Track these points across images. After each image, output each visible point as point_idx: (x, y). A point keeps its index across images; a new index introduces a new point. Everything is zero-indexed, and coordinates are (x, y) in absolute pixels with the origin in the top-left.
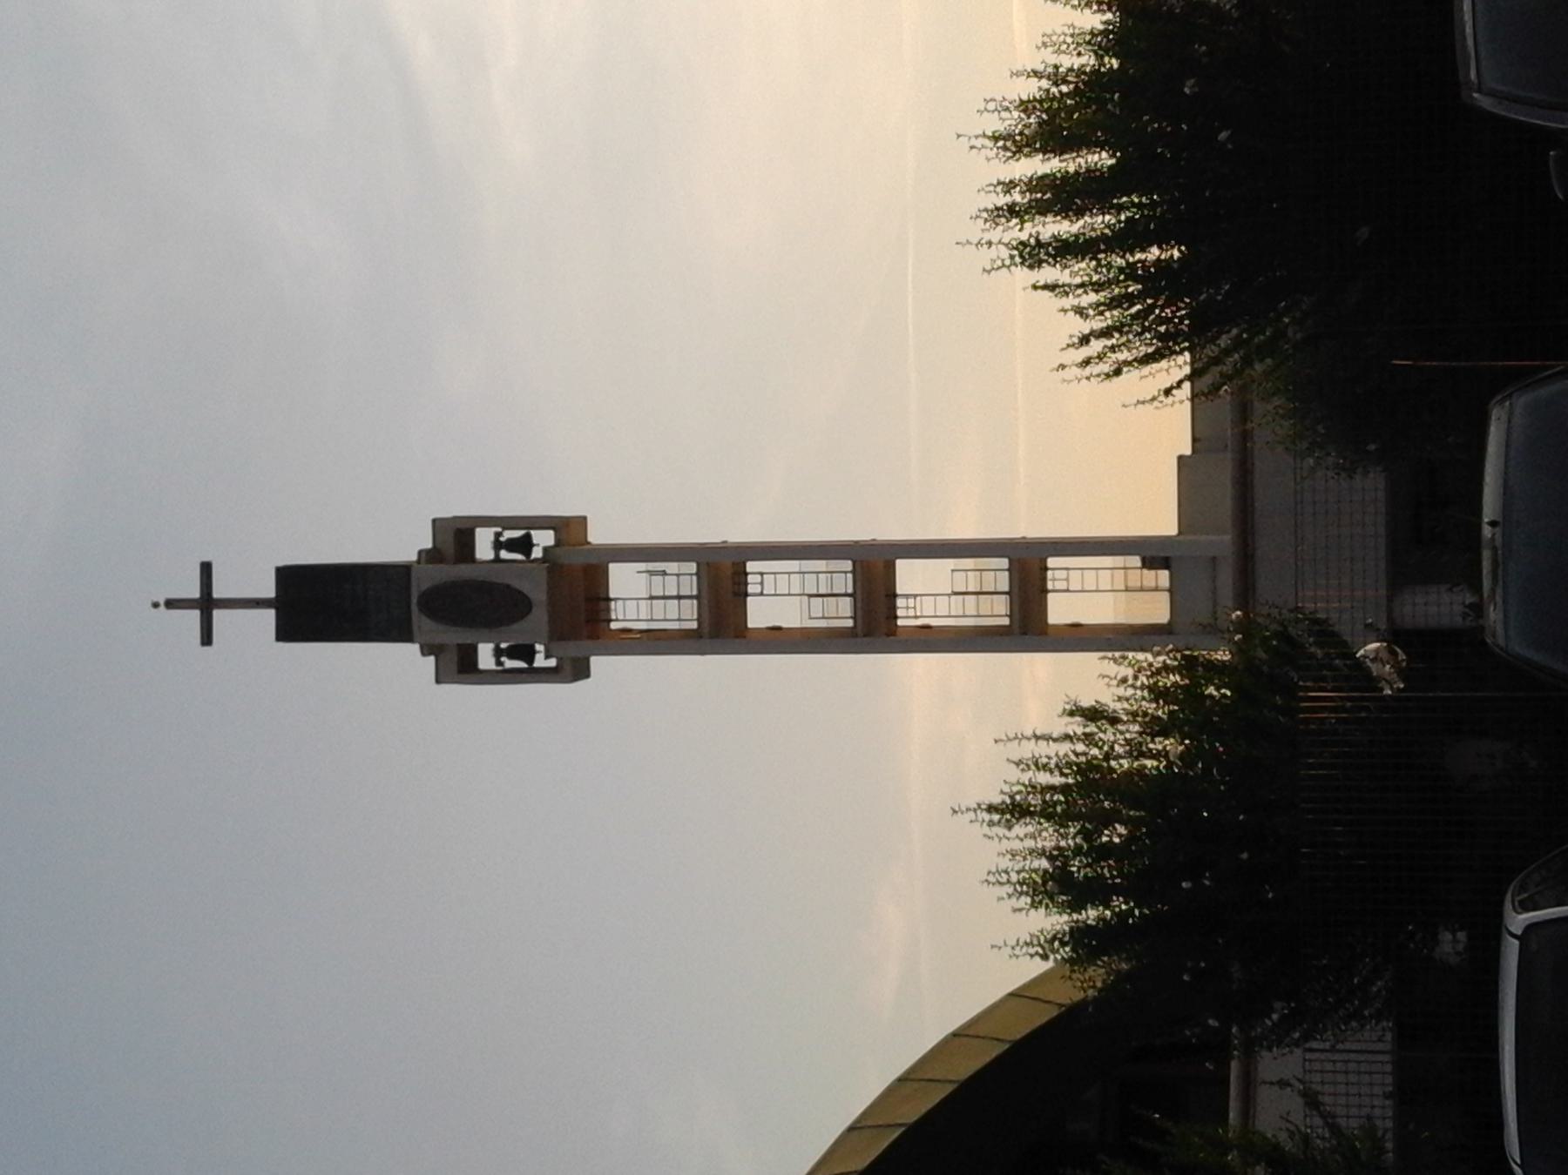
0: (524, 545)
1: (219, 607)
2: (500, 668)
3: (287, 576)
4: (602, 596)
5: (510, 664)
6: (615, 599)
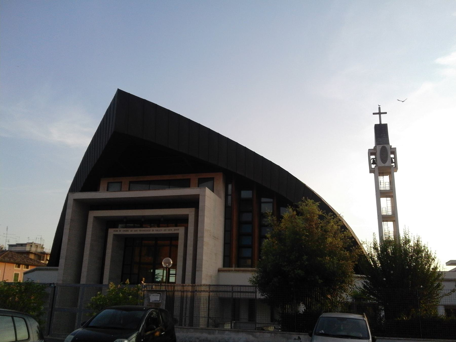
0: (392, 162)
1: (382, 114)
2: (371, 159)
3: (386, 126)
4: (384, 175)
5: (372, 161)
6: (383, 177)
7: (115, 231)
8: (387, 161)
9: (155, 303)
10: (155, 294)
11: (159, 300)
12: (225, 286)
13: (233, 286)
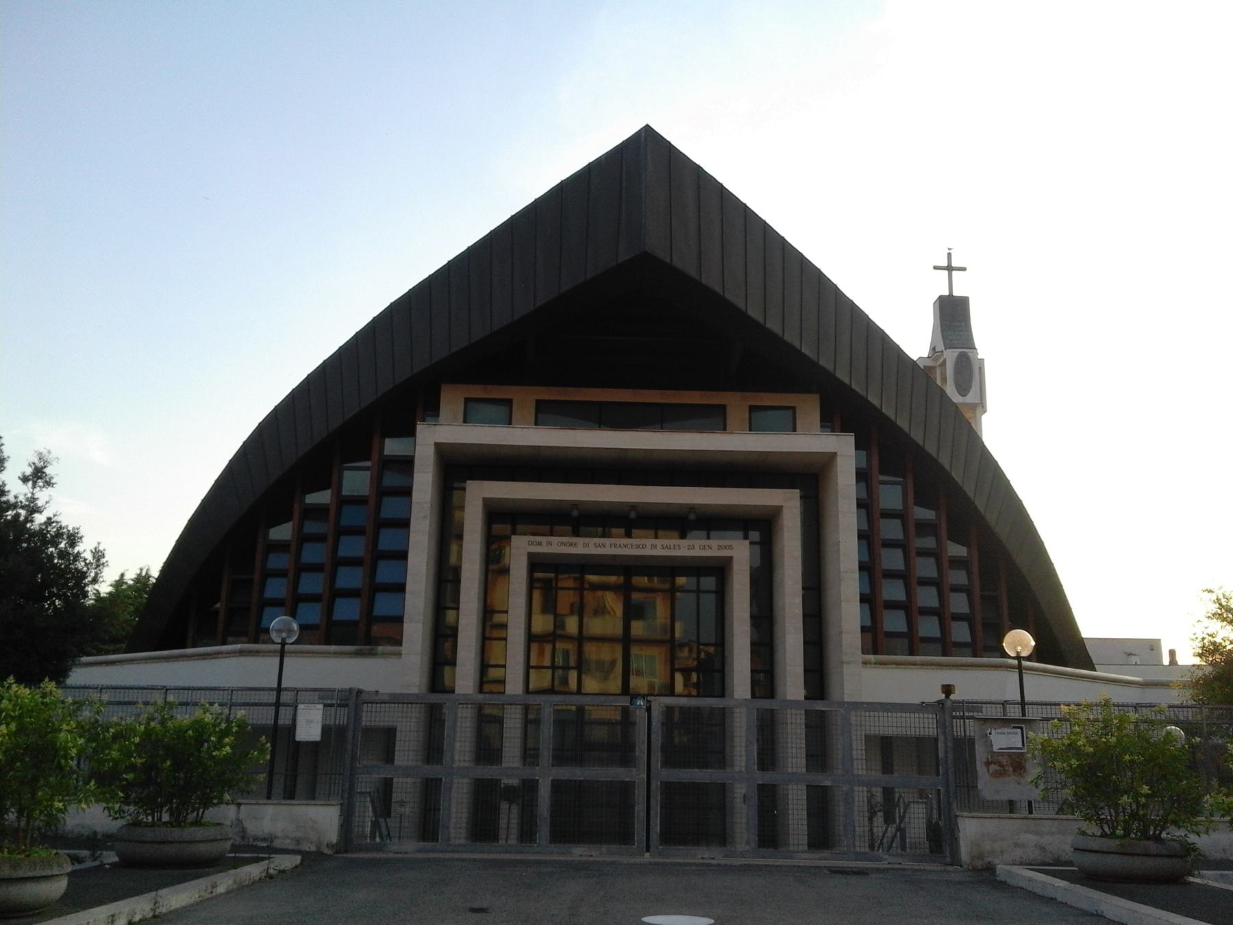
7: (532, 544)
8: (969, 391)
9: (1010, 755)
10: (1005, 730)
11: (1021, 746)
12: (188, 689)
13: (167, 690)
